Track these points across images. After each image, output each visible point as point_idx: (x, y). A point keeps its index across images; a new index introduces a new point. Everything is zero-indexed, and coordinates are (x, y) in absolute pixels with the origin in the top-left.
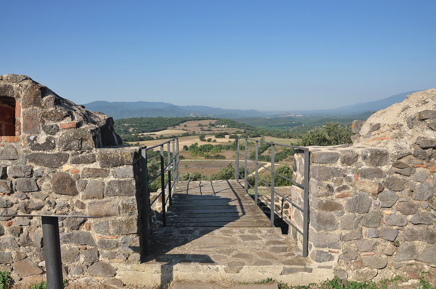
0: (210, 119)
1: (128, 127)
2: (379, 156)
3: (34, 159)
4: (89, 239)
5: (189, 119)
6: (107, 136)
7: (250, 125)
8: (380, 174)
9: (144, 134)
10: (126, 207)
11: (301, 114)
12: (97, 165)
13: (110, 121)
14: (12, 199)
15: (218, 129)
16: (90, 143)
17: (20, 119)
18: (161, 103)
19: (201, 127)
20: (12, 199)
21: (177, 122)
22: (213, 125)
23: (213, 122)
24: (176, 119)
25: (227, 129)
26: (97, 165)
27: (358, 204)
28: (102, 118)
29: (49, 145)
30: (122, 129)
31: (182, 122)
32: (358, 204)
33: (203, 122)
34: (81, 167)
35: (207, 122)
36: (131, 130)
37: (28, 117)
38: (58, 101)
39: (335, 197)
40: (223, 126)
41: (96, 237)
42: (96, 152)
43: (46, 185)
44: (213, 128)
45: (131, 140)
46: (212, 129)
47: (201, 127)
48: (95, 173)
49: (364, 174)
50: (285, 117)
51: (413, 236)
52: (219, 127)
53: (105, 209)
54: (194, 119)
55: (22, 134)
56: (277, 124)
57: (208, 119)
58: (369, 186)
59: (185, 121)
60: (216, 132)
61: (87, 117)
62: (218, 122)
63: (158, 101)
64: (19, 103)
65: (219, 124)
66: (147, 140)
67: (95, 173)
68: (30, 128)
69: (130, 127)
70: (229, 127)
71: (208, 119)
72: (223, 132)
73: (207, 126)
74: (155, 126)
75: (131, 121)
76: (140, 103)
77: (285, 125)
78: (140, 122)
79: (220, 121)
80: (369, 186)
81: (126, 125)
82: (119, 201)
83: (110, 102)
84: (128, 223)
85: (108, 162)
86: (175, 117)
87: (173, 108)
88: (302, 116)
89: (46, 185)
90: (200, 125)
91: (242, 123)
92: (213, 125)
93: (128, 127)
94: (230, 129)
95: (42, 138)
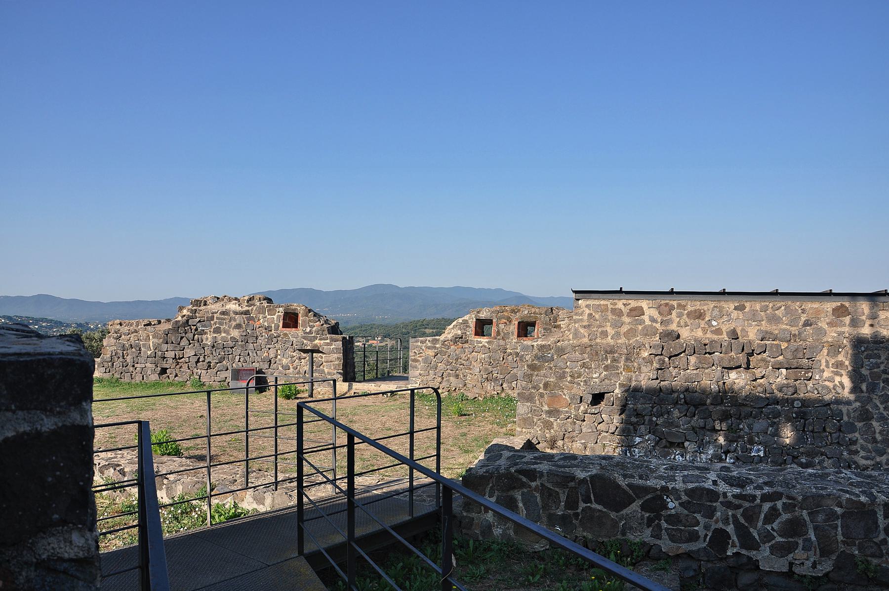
3: (304, 338)
4: (323, 371)
6: (334, 330)
8: (435, 348)
10: (338, 358)
12: (328, 341)
13: (337, 324)
14: (294, 354)
16: (326, 332)
17: (300, 322)
18: (499, 291)
20: (294, 354)
26: (328, 341)
27: (426, 360)
28: (333, 322)
29: (311, 332)
32: (426, 360)
34: (322, 342)
37: (303, 321)
38: (315, 315)
39: (417, 357)
41: (326, 370)
42: (328, 336)
48: (328, 344)
49: (429, 348)
51: (449, 375)
53: (330, 359)
55: (300, 328)
58: (431, 353)
61: (326, 322)
63: (493, 287)
64: (300, 315)
67: (328, 344)
68: (304, 326)
76: (457, 289)
80: (431, 353)
82: (336, 356)
83: (402, 283)
84: (339, 365)
85: (332, 340)
95: (308, 330)
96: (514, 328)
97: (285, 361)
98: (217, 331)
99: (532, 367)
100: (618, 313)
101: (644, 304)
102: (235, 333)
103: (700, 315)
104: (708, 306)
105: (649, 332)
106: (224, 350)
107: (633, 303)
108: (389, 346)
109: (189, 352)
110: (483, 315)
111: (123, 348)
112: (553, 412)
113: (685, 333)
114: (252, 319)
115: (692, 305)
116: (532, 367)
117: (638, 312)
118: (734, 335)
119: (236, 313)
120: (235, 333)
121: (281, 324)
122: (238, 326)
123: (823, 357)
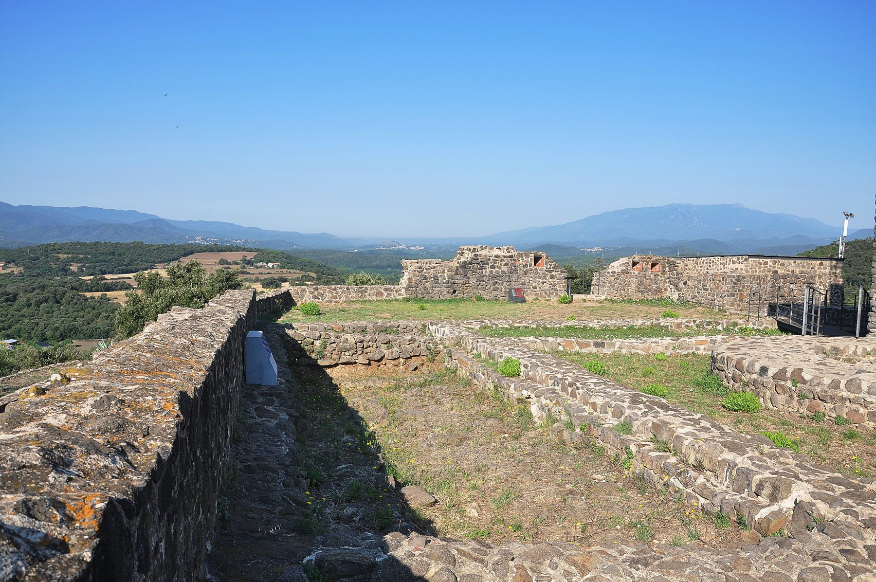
0: (244, 250)
1: (69, 262)
2: (614, 272)
5: (198, 249)
7: (323, 264)
9: (107, 276)
11: (420, 246)
15: (260, 270)
19: (226, 266)
21: (175, 255)
22: (249, 263)
23: (250, 256)
24: (172, 248)
25: (280, 270)
27: (610, 282)
30: (54, 266)
31: (185, 255)
32: (610, 282)
33: (229, 256)
35: (237, 256)
36: (74, 268)
40: (270, 265)
43: (548, 277)
44: (250, 269)
45: (85, 288)
46: (248, 271)
47: (226, 266)
50: (390, 251)
52: (261, 267)
54: (210, 249)
56: (374, 263)
57: (238, 249)
58: (612, 278)
59: (192, 253)
60: (262, 277)
62: (261, 257)
65: (262, 261)
66: (120, 289)
69: (73, 261)
70: (281, 267)
71: (238, 249)
72: (276, 276)
73: (237, 263)
74: (127, 262)
75: (75, 248)
77: (389, 266)
78: (93, 251)
79: (264, 255)
80: (612, 278)
81: (62, 256)
83: (15, 204)
86: (161, 242)
87: (158, 224)
88: (422, 248)
89: (548, 277)
90: (222, 262)
91: (307, 259)
92: (249, 263)
93: (69, 262)
94: (285, 270)
96: (649, 266)
97: (534, 284)
98: (493, 267)
99: (735, 284)
100: (760, 263)
101: (768, 260)
102: (504, 269)
103: (783, 265)
104: (786, 261)
105: (769, 271)
106: (496, 279)
107: (765, 260)
108: (16, 273)
109: (473, 280)
110: (635, 260)
111: (426, 278)
112: (741, 301)
113: (779, 271)
114: (515, 260)
115: (782, 261)
116: (735, 284)
117: (766, 263)
118: (793, 272)
119: (504, 257)
120: (504, 269)
121: (533, 263)
122: (506, 265)
123: (817, 279)
